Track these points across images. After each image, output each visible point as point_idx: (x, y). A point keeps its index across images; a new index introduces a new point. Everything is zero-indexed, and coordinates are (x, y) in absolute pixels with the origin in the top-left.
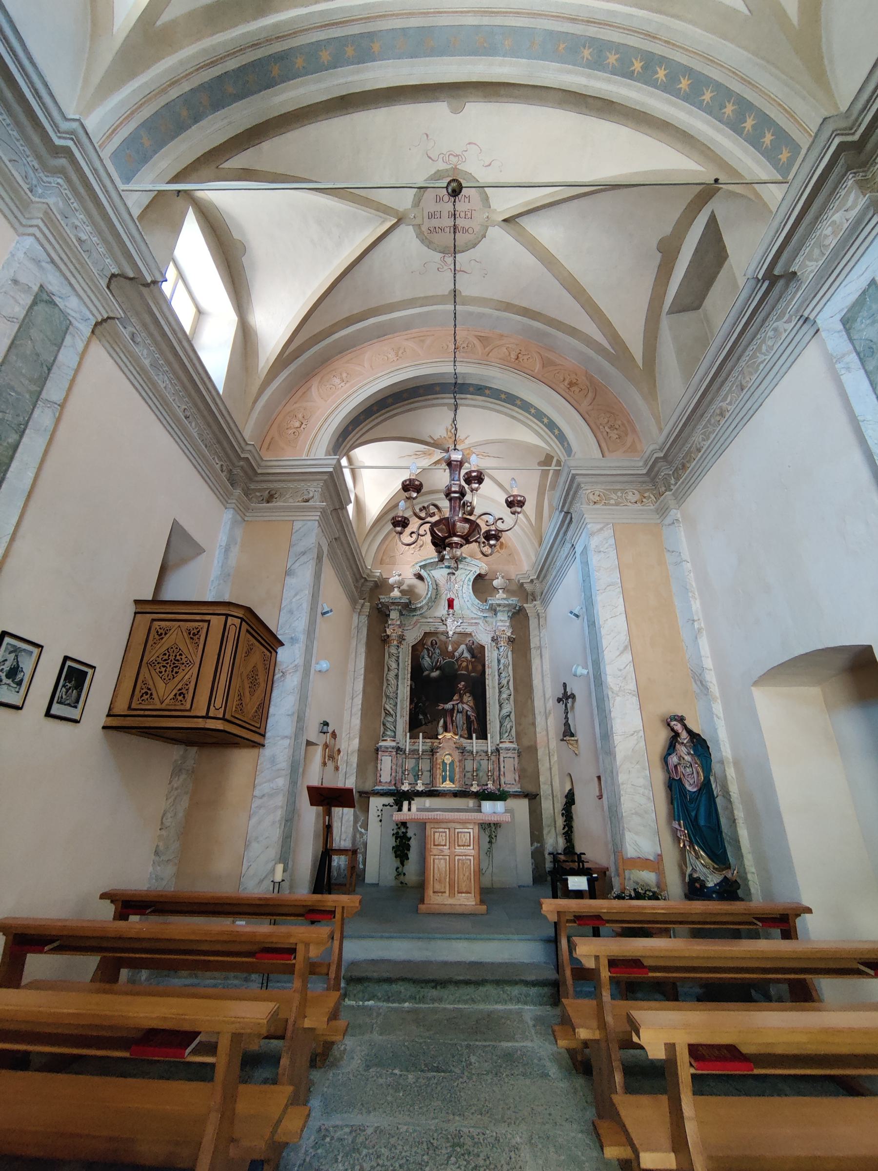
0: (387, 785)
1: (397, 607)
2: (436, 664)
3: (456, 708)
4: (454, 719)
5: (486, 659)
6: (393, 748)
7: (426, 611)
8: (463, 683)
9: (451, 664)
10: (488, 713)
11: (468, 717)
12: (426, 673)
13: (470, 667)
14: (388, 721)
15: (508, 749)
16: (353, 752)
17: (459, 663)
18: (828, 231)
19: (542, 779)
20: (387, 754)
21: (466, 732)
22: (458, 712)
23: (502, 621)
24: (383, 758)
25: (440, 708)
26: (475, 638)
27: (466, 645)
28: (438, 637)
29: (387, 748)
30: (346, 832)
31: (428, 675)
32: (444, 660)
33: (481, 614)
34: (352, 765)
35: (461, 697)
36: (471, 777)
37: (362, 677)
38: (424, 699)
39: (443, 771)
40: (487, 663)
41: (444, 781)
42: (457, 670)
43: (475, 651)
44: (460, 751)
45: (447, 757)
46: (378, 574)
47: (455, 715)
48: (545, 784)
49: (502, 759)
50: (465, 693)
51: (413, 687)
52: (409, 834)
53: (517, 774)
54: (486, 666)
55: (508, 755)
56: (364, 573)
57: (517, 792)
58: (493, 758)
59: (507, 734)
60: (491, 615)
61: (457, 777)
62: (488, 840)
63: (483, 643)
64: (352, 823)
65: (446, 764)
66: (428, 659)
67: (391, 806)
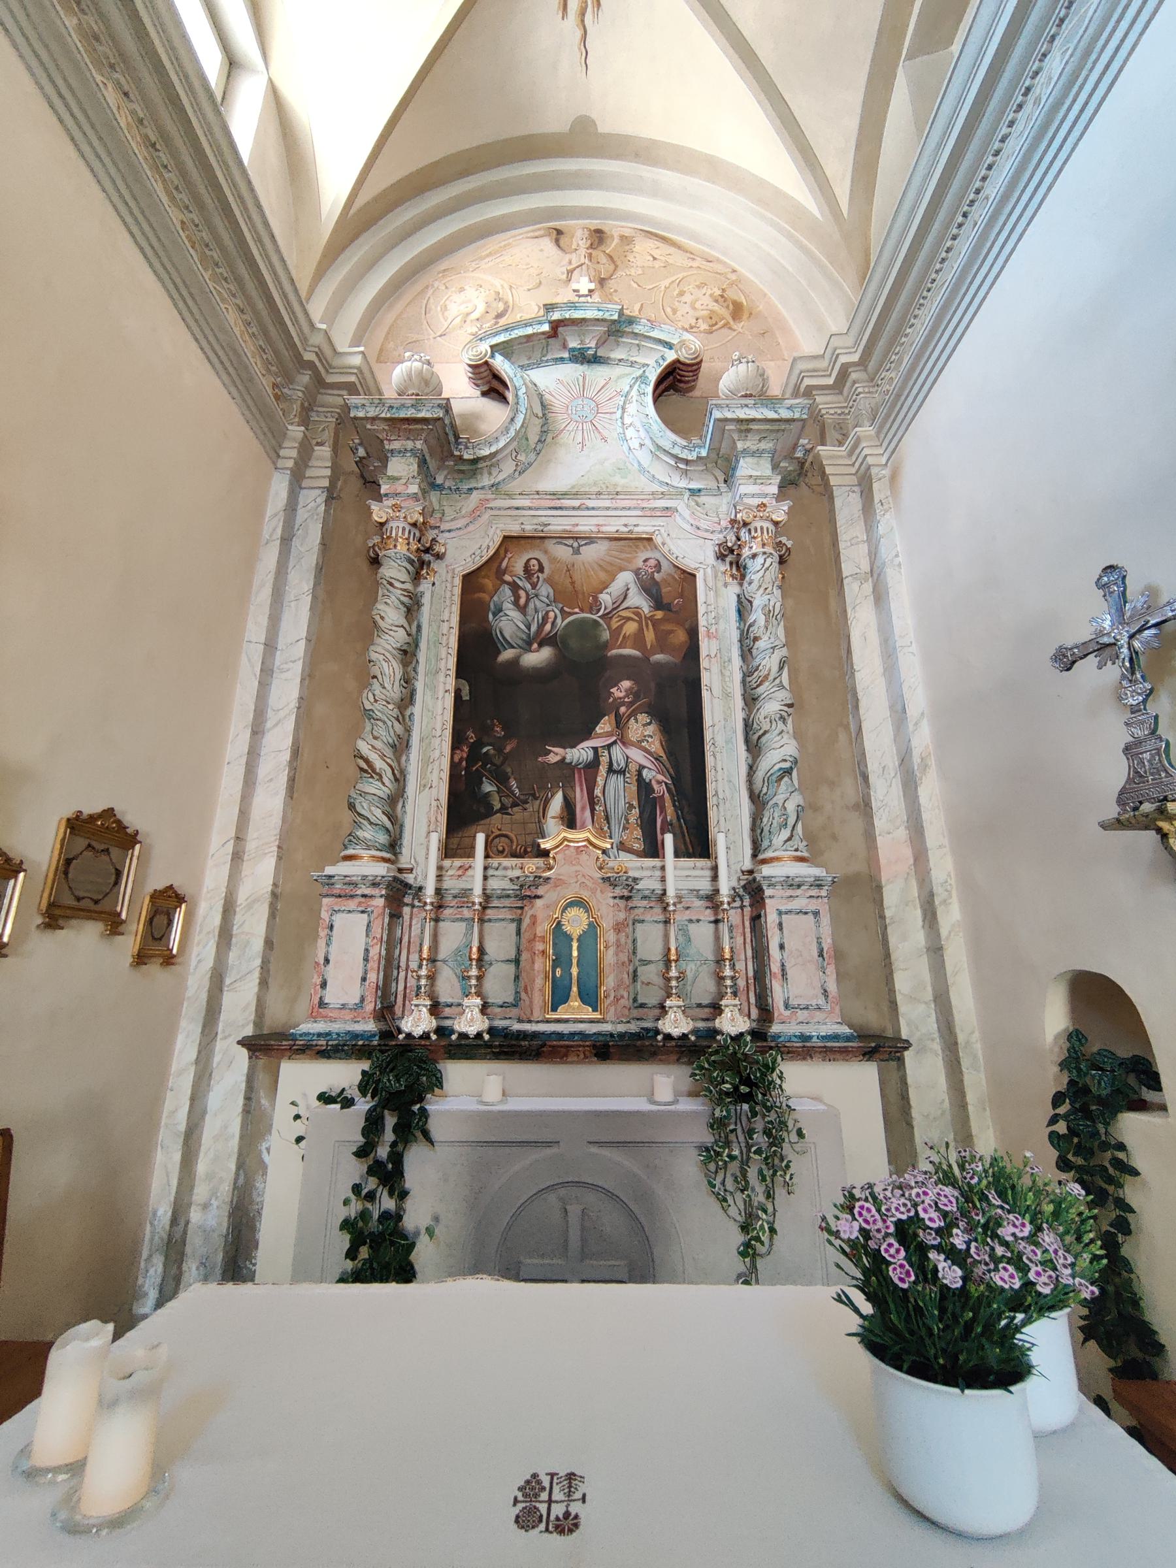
0: (348, 1015)
1: (409, 444)
2: (541, 626)
3: (604, 760)
4: (598, 792)
5: (701, 609)
6: (375, 885)
7: (511, 477)
8: (626, 684)
9: (586, 629)
10: (710, 775)
11: (644, 787)
12: (507, 655)
13: (650, 636)
14: (363, 794)
15: (792, 884)
16: (252, 903)
17: (614, 625)
18: (856, 586)
19: (902, 983)
20: (352, 904)
21: (638, 833)
22: (611, 770)
23: (755, 479)
24: (338, 919)
25: (553, 759)
26: (665, 549)
27: (637, 572)
28: (546, 552)
29: (355, 885)
30: (210, 1177)
31: (515, 662)
32: (565, 614)
33: (683, 484)
34: (247, 944)
35: (620, 724)
36: (659, 981)
37: (298, 667)
38: (499, 731)
39: (556, 963)
40: (702, 622)
41: (559, 997)
42: (606, 646)
43: (664, 590)
44: (618, 891)
45: (573, 912)
46: (357, 361)
47: (600, 781)
48: (913, 999)
49: (771, 918)
50: (633, 714)
51: (466, 697)
52: (415, 1217)
53: (831, 970)
54: (702, 631)
55: (795, 905)
56: (304, 340)
57: (835, 1037)
58: (734, 916)
59: (785, 834)
60: (713, 485)
61: (609, 982)
62: (739, 1238)
63: (689, 564)
64: (234, 1143)
65: (569, 938)
66: (514, 614)
67: (348, 1103)
